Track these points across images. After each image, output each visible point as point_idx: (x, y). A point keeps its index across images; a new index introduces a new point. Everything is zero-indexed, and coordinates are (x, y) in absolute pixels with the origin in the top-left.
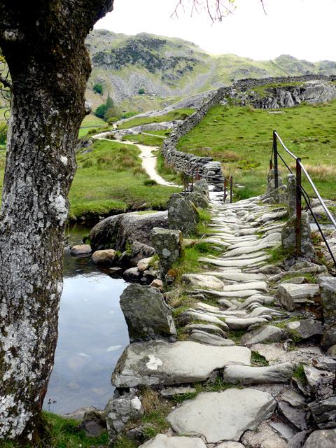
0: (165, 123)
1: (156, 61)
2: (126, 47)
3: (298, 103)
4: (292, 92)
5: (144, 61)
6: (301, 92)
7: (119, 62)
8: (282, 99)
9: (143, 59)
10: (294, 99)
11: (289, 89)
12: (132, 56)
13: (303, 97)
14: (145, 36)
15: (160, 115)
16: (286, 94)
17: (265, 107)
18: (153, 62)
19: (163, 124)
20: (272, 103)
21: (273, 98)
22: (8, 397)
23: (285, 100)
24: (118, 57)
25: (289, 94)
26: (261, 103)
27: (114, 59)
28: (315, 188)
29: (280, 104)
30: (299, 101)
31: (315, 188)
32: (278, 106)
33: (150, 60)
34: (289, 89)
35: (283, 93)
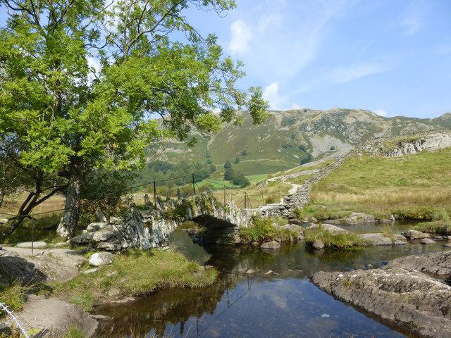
1: (343, 127)
8: (405, 150)
9: (334, 126)
10: (416, 148)
11: (412, 141)
24: (315, 125)
30: (421, 150)
34: (412, 141)
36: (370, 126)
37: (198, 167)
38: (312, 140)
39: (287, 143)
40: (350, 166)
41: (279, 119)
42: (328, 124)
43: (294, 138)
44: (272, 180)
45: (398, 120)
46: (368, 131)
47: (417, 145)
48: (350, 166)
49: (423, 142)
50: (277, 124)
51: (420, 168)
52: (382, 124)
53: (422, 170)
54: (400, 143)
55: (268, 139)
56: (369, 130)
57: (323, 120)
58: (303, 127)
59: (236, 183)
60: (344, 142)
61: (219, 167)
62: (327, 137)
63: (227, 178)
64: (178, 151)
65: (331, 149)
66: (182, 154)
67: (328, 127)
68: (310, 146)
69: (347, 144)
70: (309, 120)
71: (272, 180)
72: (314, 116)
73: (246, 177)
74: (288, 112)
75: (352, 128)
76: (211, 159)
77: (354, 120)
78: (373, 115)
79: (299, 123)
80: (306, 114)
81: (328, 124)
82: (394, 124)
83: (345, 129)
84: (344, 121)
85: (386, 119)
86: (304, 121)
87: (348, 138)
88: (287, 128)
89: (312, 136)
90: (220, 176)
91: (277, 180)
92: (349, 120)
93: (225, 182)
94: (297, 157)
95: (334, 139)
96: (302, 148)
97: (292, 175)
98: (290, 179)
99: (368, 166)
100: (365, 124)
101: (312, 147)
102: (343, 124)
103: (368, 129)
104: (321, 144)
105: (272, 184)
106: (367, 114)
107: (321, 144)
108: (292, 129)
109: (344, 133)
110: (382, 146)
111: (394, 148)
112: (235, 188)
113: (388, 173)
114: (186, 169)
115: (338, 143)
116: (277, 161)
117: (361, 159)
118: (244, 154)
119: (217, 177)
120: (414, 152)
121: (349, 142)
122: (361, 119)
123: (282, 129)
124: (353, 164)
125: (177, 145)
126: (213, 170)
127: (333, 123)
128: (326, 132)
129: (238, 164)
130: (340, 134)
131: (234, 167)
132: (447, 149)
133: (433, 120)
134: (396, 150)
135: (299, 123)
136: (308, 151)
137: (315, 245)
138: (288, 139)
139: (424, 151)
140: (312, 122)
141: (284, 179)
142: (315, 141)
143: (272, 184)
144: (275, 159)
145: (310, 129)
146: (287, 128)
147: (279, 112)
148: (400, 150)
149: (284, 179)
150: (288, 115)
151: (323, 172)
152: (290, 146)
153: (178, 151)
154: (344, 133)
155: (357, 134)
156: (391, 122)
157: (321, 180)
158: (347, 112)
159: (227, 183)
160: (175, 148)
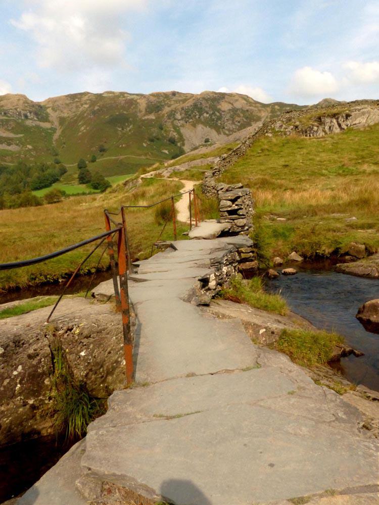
0: (212, 158)
1: (218, 114)
2: (192, 104)
3: (344, 129)
4: (337, 119)
5: (208, 115)
6: (347, 118)
7: (188, 118)
8: (327, 128)
9: (207, 113)
10: (340, 125)
11: (334, 116)
12: (198, 112)
13: (348, 123)
14: (207, 93)
15: (207, 151)
16: (331, 122)
17: (310, 136)
18: (215, 116)
19: (210, 159)
20: (317, 131)
21: (318, 127)
22: (255, 279)
23: (330, 127)
24: (186, 113)
25: (334, 121)
26: (306, 132)
27: (183, 115)
28: (70, 280)
29: (326, 133)
30: (345, 127)
31: (70, 280)
32: (324, 134)
33: (213, 114)
34: (334, 116)
35: (328, 120)
36: (247, 114)
37: (43, 169)
38: (182, 130)
39: (154, 135)
40: (262, 150)
41: (143, 104)
42: (201, 111)
43: (161, 128)
44: (148, 175)
45: (277, 107)
46: (245, 120)
47: (341, 120)
48: (262, 150)
49: (348, 116)
50: (140, 111)
51: (356, 151)
52: (260, 111)
53: (360, 153)
54: (320, 118)
55: (130, 130)
56: (247, 118)
57: (195, 106)
58: (172, 115)
59: (96, 188)
60: (219, 133)
61: (71, 167)
62: (200, 127)
63: (83, 180)
64: (13, 148)
65: (205, 142)
66: (19, 153)
67: (200, 115)
68: (181, 138)
69: (222, 136)
70: (179, 106)
71: (148, 175)
72: (184, 101)
73: (106, 179)
74: (152, 95)
75: (228, 116)
76: (58, 158)
77: (230, 107)
78: (250, 100)
79: (167, 110)
80: (175, 98)
81: (201, 111)
82: (273, 111)
83: (219, 118)
84: (219, 107)
85: (264, 106)
86: (173, 107)
87: (224, 128)
88: (152, 117)
89: (183, 126)
90: (74, 179)
91: (156, 175)
92: (225, 106)
93: (80, 186)
94: (166, 152)
95: (208, 129)
96: (172, 141)
97: (178, 167)
98: (176, 174)
99: (286, 151)
100: (243, 111)
101: (184, 140)
102: (219, 110)
103: (244, 116)
104: (193, 135)
105: (148, 182)
106: (245, 99)
107: (193, 135)
108: (158, 118)
109: (219, 122)
110: (298, 123)
111: (313, 125)
112: (94, 193)
113: (318, 159)
114: (27, 172)
115: (213, 134)
116: (143, 157)
117: (274, 140)
118: (102, 150)
119: (69, 181)
120: (337, 130)
121: (225, 134)
122: (238, 105)
123: (146, 117)
124: (266, 147)
125: (11, 139)
126: (64, 171)
127: (207, 109)
128: (199, 121)
129: (95, 163)
130: (215, 123)
131: (91, 167)
132: (376, 125)
133: (312, 107)
134: (315, 128)
135: (167, 110)
136: (179, 144)
137: (5, 203)
138: (155, 131)
139: (350, 130)
140: (182, 109)
141: (166, 174)
142: (187, 132)
143: (148, 182)
144: (140, 155)
145: (180, 117)
146: (152, 117)
147: (142, 95)
148: (321, 128)
149: (166, 174)
150: (152, 99)
151: (228, 160)
152: (158, 139)
153: (13, 148)
154: (219, 122)
155: (233, 123)
156: (269, 109)
157: (226, 171)
158: (222, 96)
159: (83, 188)
160: (9, 145)
